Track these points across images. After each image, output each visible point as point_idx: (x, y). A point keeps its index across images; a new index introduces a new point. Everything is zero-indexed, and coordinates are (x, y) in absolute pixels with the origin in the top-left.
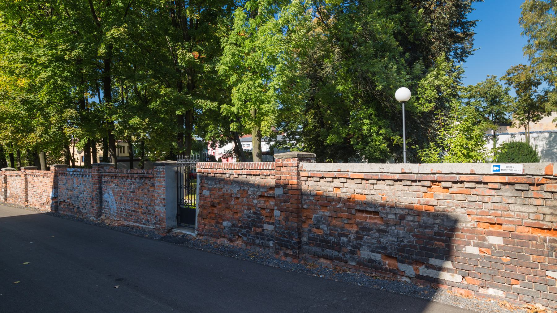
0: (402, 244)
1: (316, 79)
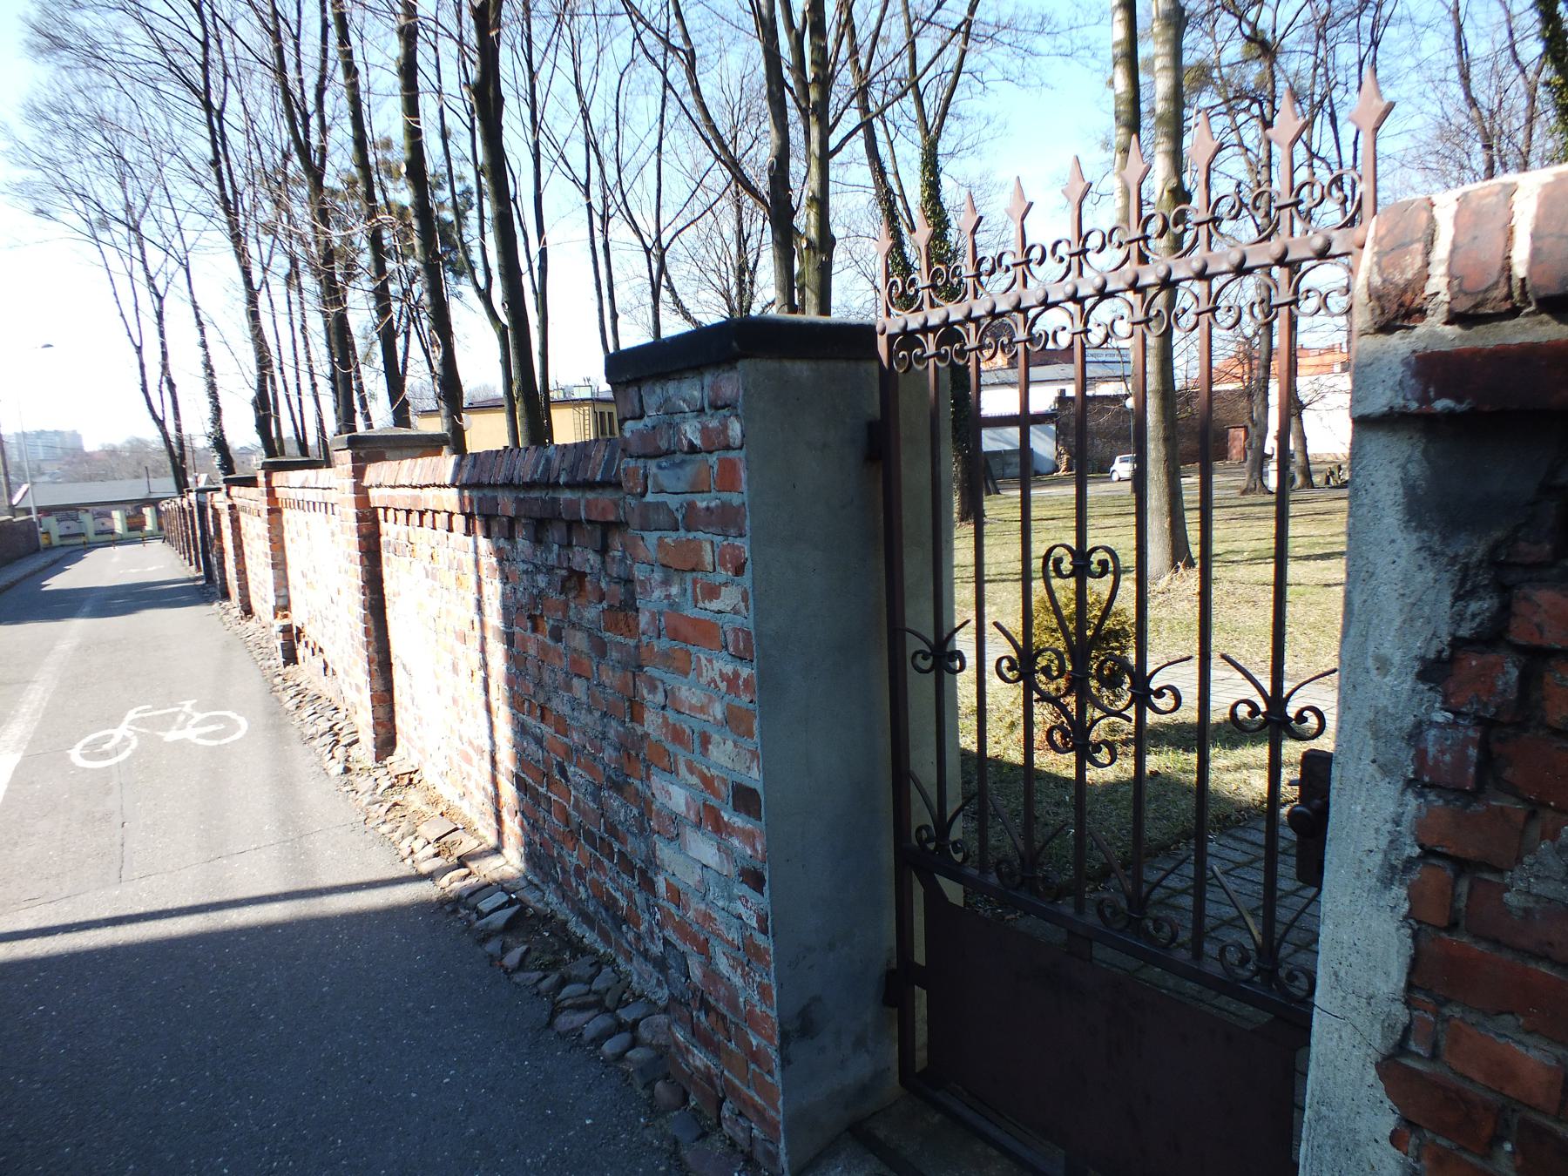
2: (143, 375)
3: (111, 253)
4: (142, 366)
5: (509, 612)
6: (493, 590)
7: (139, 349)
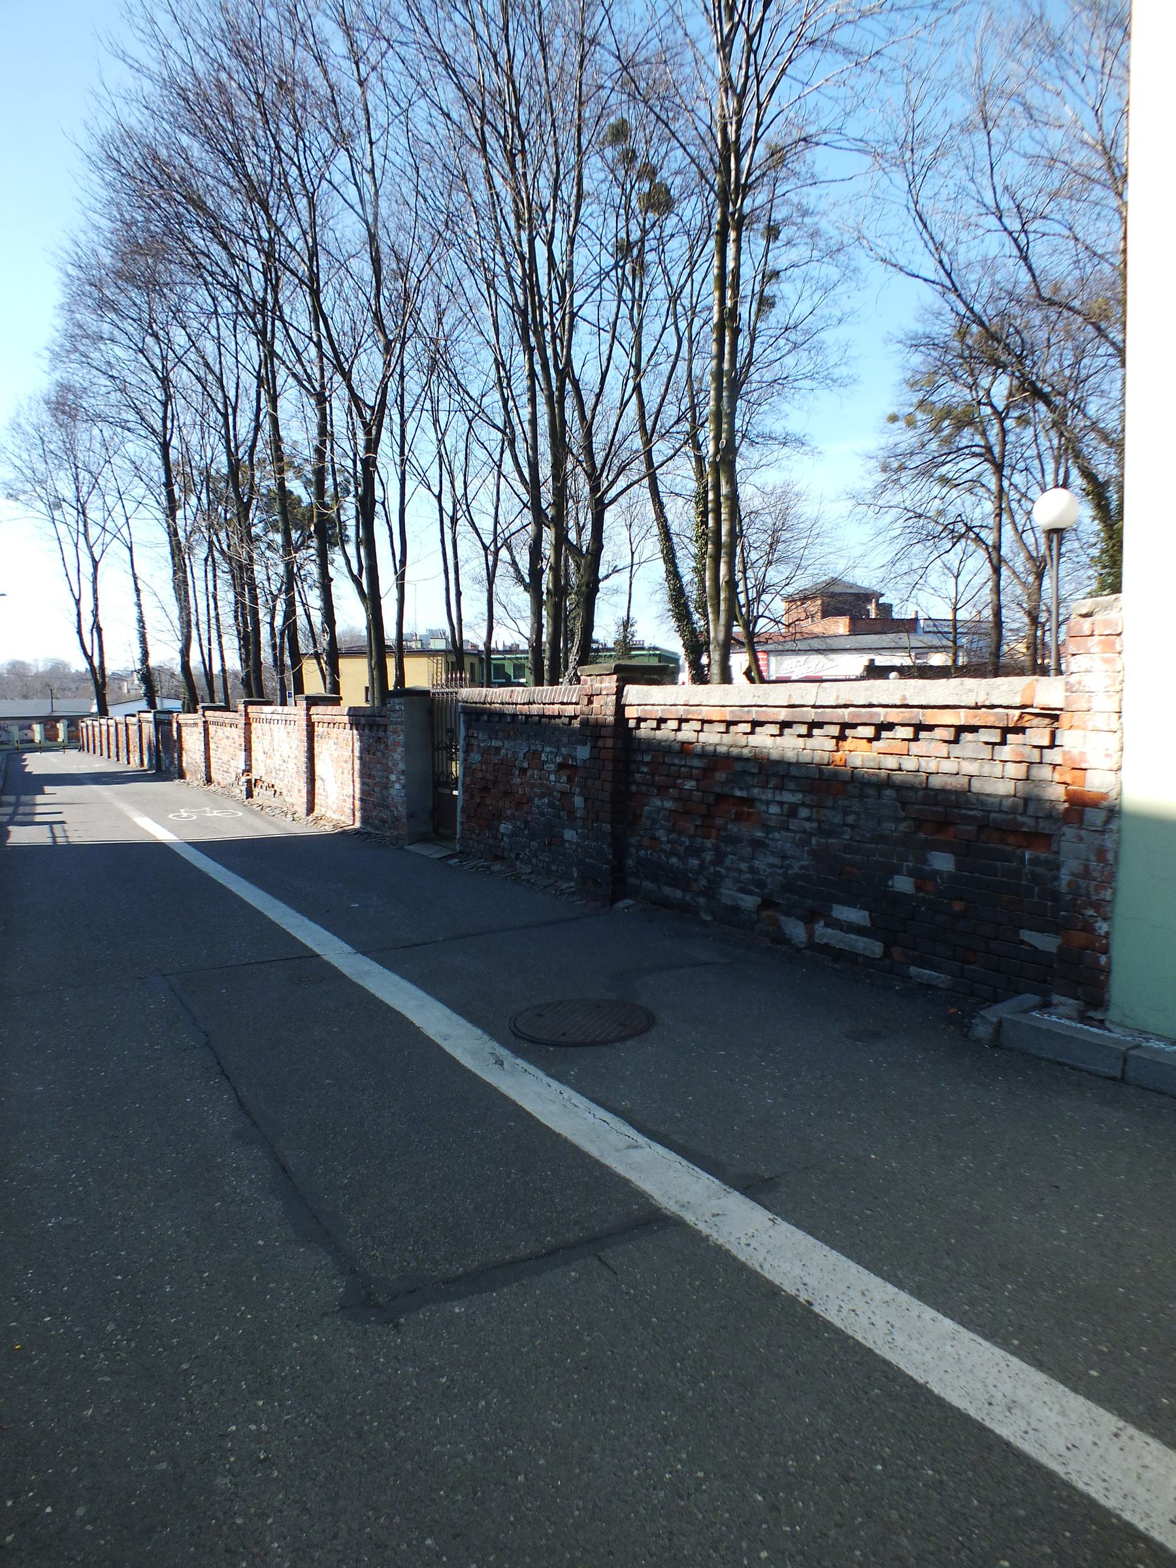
0: (790, 872)
2: (79, 621)
3: (63, 529)
4: (79, 615)
5: (362, 751)
6: (357, 745)
7: (78, 602)
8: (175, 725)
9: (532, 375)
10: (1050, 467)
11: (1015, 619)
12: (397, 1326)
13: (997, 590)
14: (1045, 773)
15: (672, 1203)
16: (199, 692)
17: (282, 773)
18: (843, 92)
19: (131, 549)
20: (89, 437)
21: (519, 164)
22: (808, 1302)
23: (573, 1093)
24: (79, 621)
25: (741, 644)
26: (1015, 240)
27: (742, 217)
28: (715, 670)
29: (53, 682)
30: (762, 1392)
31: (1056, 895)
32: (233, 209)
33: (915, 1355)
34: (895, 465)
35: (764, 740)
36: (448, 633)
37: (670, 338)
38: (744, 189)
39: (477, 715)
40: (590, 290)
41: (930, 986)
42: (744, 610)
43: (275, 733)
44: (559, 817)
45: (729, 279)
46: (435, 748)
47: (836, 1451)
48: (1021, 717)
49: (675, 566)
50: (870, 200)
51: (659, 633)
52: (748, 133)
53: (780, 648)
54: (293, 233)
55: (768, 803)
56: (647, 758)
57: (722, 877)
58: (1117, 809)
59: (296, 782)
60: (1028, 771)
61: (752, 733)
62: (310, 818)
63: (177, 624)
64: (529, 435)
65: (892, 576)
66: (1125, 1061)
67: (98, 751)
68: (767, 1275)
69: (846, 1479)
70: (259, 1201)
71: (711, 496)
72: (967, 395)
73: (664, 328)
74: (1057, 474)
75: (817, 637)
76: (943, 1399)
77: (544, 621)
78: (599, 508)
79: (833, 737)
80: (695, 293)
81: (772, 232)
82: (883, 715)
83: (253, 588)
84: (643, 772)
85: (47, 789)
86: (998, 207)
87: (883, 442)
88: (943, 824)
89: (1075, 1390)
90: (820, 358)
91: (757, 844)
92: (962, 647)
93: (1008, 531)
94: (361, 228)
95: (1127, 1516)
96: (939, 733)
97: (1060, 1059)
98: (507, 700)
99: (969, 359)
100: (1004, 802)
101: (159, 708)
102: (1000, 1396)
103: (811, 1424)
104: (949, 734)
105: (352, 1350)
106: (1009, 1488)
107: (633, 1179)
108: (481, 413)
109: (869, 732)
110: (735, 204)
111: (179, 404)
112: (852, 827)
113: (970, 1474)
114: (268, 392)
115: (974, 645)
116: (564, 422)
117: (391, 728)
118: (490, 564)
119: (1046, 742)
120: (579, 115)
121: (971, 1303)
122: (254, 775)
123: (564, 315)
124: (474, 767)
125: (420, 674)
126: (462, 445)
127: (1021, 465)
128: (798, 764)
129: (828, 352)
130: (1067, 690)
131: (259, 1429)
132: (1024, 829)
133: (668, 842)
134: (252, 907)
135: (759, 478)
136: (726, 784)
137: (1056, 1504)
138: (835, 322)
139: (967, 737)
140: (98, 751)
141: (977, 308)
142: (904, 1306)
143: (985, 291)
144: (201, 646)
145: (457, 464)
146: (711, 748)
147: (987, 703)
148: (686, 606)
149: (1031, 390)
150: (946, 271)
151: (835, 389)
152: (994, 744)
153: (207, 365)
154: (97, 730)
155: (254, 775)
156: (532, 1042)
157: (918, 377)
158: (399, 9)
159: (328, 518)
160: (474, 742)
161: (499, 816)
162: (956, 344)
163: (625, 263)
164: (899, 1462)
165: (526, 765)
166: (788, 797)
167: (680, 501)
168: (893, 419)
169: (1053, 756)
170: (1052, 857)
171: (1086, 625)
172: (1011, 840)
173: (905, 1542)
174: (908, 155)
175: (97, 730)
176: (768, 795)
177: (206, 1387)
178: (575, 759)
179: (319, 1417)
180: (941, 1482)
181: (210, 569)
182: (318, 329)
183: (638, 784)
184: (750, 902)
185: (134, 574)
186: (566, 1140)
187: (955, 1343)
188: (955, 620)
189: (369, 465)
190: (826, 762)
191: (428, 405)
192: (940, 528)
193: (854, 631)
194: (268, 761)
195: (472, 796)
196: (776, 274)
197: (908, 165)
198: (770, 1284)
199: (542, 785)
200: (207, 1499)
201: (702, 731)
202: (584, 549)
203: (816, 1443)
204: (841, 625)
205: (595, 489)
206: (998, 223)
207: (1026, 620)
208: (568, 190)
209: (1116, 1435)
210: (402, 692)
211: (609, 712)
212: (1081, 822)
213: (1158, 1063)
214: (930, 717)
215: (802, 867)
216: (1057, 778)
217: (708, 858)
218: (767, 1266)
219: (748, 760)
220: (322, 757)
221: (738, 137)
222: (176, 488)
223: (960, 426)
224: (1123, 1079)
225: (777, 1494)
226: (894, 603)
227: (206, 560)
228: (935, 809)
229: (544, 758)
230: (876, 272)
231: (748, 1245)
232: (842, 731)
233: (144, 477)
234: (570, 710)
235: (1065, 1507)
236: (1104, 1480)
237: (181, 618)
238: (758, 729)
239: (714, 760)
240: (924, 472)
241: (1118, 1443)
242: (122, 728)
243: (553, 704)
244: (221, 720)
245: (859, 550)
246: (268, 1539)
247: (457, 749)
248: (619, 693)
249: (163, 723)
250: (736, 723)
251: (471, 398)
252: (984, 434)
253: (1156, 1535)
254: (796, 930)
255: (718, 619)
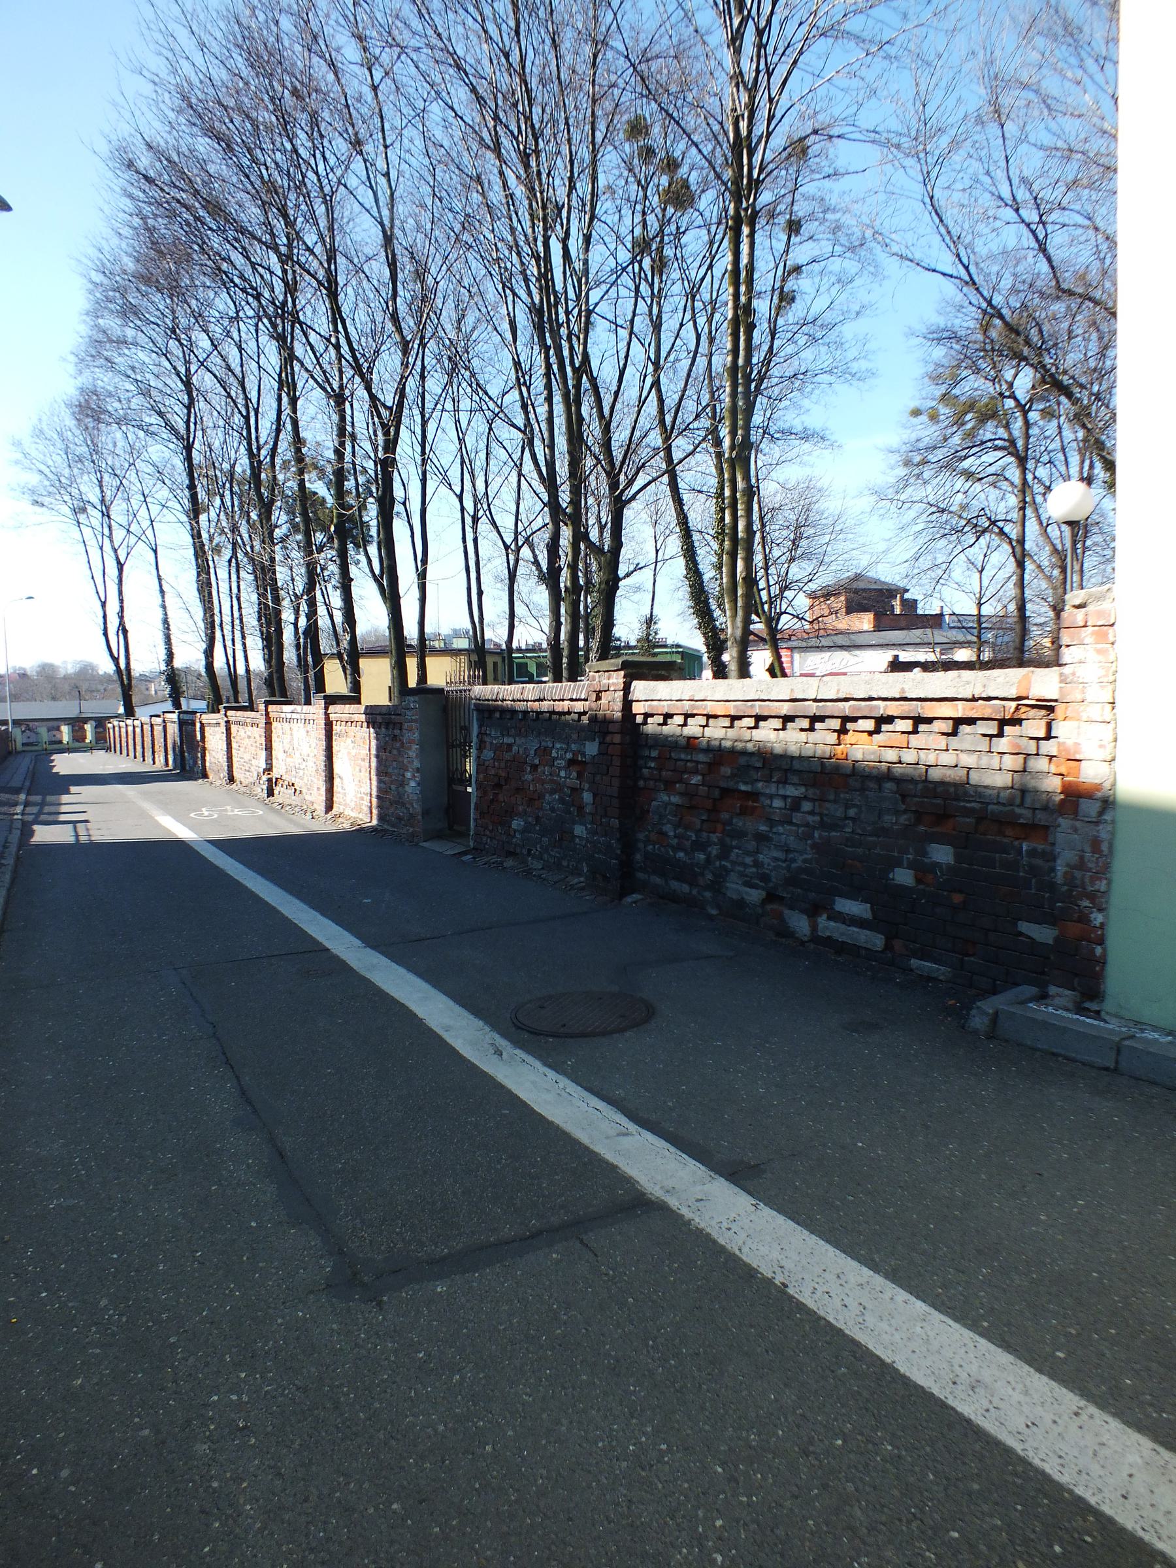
0: (793, 865)
1: (150, 230)
2: (105, 623)
3: (87, 532)
4: (105, 617)
6: (374, 743)
7: (104, 604)
8: (198, 725)
9: (548, 374)
10: (1074, 459)
11: (1039, 612)
12: (380, 1304)
13: (1021, 584)
14: (1041, 764)
15: (657, 1188)
16: (225, 693)
17: (301, 772)
18: (855, 82)
19: (155, 551)
20: (114, 438)
21: (533, 163)
22: (783, 1284)
23: (568, 1082)
24: (105, 623)
25: (763, 640)
26: (1033, 232)
27: (755, 214)
28: (733, 667)
29: (81, 684)
30: (730, 1369)
31: (1052, 886)
32: (251, 214)
33: (884, 1336)
34: (917, 459)
35: (767, 734)
36: (471, 633)
37: (688, 332)
38: (755, 185)
39: (490, 712)
40: (604, 287)
41: (930, 979)
42: (766, 607)
43: (294, 732)
44: (570, 813)
45: (743, 275)
46: (450, 746)
47: (798, 1426)
48: (1017, 709)
49: (696, 564)
50: (882, 197)
51: (680, 630)
52: (760, 128)
53: (804, 644)
54: (311, 238)
55: (771, 797)
56: (654, 754)
57: (728, 871)
58: (1111, 799)
59: (315, 780)
60: (1025, 763)
61: (756, 727)
62: (329, 816)
63: (202, 625)
64: (546, 435)
65: (916, 571)
66: (1119, 1052)
67: (125, 752)
68: (744, 1258)
69: (806, 1453)
70: (254, 1185)
71: (727, 493)
72: (990, 389)
73: (681, 325)
74: (1082, 468)
75: (841, 633)
76: (908, 1378)
77: (563, 619)
78: (619, 506)
79: (835, 731)
80: (716, 286)
81: (794, 227)
82: (883, 708)
83: (275, 590)
84: (650, 768)
85: (73, 789)
86: (1014, 199)
87: (905, 437)
88: (942, 817)
89: (1040, 1371)
90: (839, 352)
91: (761, 838)
92: (985, 642)
93: (1032, 527)
94: (377, 232)
95: (1079, 1491)
96: (938, 726)
97: (1055, 1050)
98: (518, 697)
99: (991, 351)
100: (1002, 794)
101: (184, 708)
102: (964, 1376)
103: (776, 1400)
104: (947, 727)
105: (334, 1326)
106: (964, 1463)
107: (620, 1165)
108: (500, 413)
109: (869, 725)
110: (747, 201)
111: (201, 404)
112: (853, 819)
113: (928, 1449)
114: (288, 394)
115: (1000, 640)
116: (581, 419)
117: (406, 726)
118: (512, 562)
119: (1042, 734)
120: (593, 112)
121: (944, 1286)
122: (275, 774)
123: (580, 310)
124: (487, 763)
125: (440, 673)
126: (482, 445)
127: (1045, 458)
128: (801, 758)
129: (846, 346)
130: (1061, 682)
131: (240, 1398)
132: (1022, 821)
133: (675, 837)
134: (267, 903)
135: (780, 474)
136: (732, 777)
137: (1010, 1478)
138: (853, 315)
139: (965, 729)
140: (125, 752)
141: (998, 300)
142: (878, 1289)
143: (1006, 283)
144: (225, 646)
145: (478, 463)
146: (717, 743)
147: (984, 695)
148: (707, 604)
149: (1053, 383)
150: (963, 265)
151: (855, 383)
152: (991, 736)
153: (229, 368)
154: (123, 730)
155: (275, 774)
156: (531, 1033)
157: (941, 370)
158: (409, 11)
159: (351, 519)
160: (487, 739)
161: (511, 813)
162: (980, 337)
163: (642, 257)
164: (859, 1437)
165: (537, 761)
166: (791, 791)
167: (702, 497)
168: (916, 413)
169: (1048, 747)
170: (1048, 848)
171: (1080, 615)
172: (1009, 832)
173: (859, 1513)
174: (919, 144)
175: (123, 730)
176: (772, 789)
177: (191, 1360)
178: (584, 755)
179: (298, 1389)
180: (899, 1457)
181: (233, 571)
182: (336, 331)
183: (645, 780)
184: (755, 896)
185: (159, 576)
186: (557, 1128)
187: (924, 1324)
188: (979, 615)
189: (387, 466)
190: (827, 755)
191: (449, 405)
192: (963, 522)
193: (878, 627)
194: (288, 760)
195: (485, 793)
196: (797, 269)
197: (922, 155)
198: (748, 1266)
199: (552, 781)
200: (185, 1464)
201: (707, 725)
202: (606, 547)
203: (779, 1419)
204: (865, 621)
205: (614, 485)
206: (1015, 215)
207: (1051, 614)
208: (583, 187)
209: (1077, 1414)
210: (423, 689)
211: (616, 708)
212: (1076, 813)
213: (1149, 1053)
214: (928, 710)
215: (805, 861)
216: (1053, 769)
217: (714, 852)
218: (745, 1250)
219: (752, 754)
220: (340, 755)
221: (750, 132)
222: (199, 489)
223: (983, 419)
224: (1116, 1070)
225: (736, 1467)
226: (919, 597)
227: (230, 561)
228: (934, 801)
229: (554, 754)
230: (892, 265)
231: (729, 1229)
232: (843, 725)
233: (167, 481)
234: (579, 707)
235: (1019, 1481)
236: (1060, 1457)
237: (205, 619)
238: (762, 724)
239: (719, 755)
240: (949, 465)
241: (1077, 1421)
242: (147, 728)
243: (563, 700)
244: (243, 720)
245: (882, 546)
246: (241, 1501)
247: (470, 747)
248: (627, 689)
249: (186, 724)
250: (740, 718)
251: (490, 397)
252: (1007, 426)
253: (1106, 1509)
254: (800, 924)
255: (741, 613)
